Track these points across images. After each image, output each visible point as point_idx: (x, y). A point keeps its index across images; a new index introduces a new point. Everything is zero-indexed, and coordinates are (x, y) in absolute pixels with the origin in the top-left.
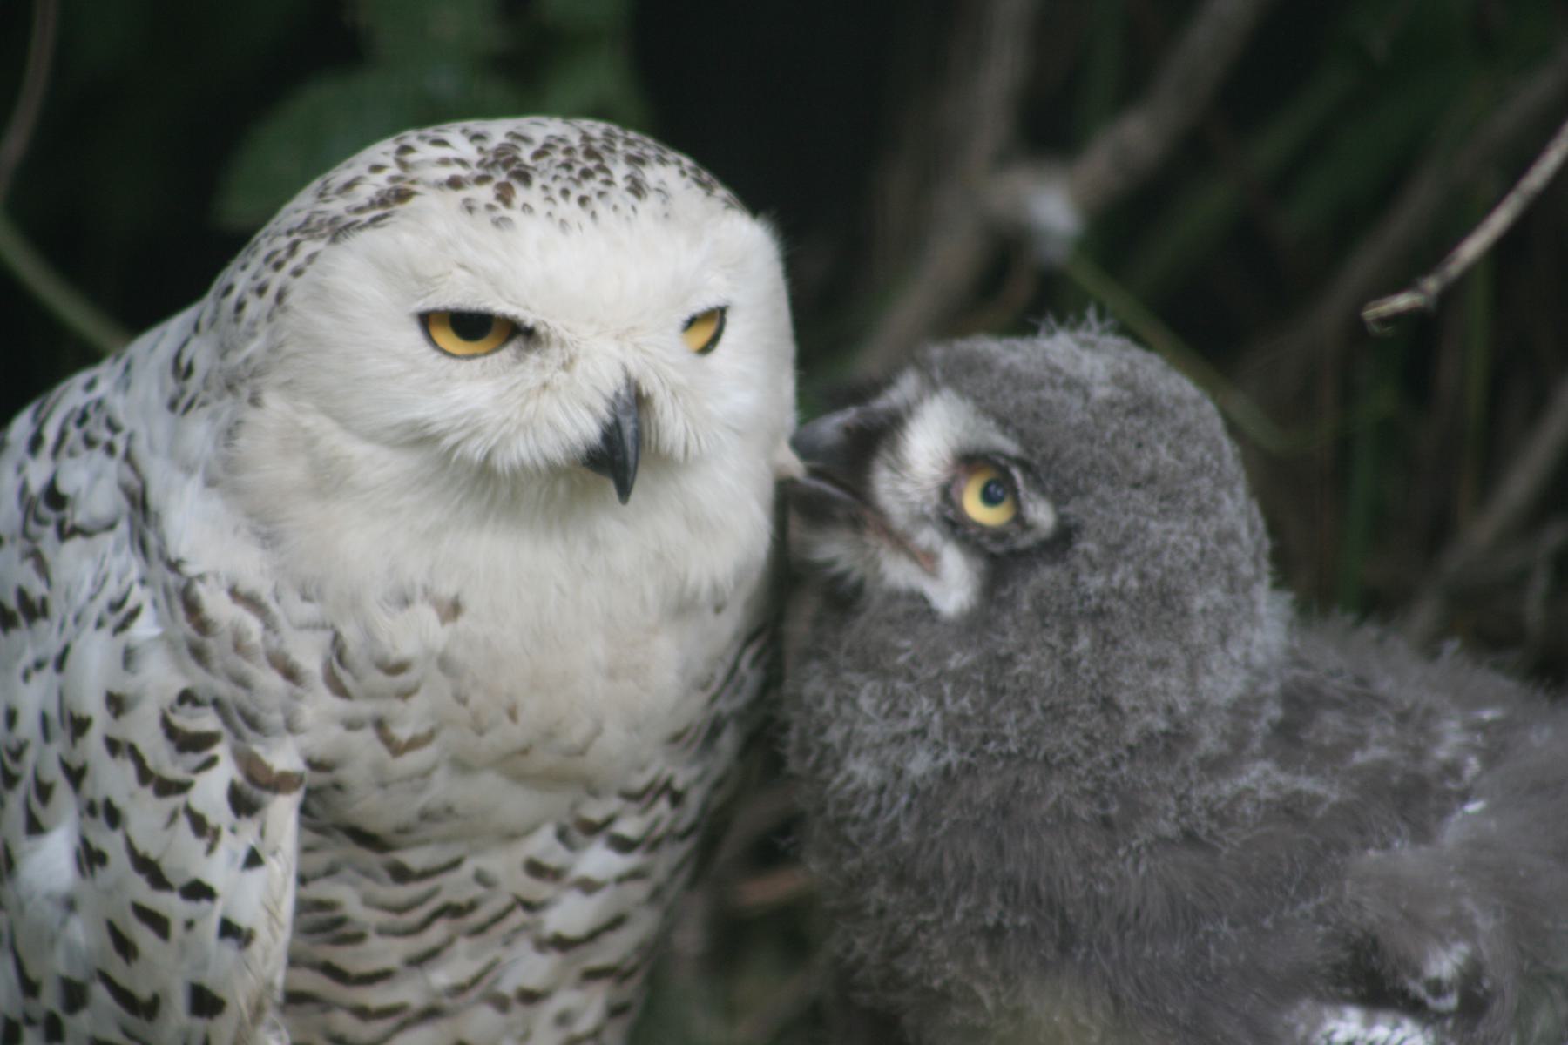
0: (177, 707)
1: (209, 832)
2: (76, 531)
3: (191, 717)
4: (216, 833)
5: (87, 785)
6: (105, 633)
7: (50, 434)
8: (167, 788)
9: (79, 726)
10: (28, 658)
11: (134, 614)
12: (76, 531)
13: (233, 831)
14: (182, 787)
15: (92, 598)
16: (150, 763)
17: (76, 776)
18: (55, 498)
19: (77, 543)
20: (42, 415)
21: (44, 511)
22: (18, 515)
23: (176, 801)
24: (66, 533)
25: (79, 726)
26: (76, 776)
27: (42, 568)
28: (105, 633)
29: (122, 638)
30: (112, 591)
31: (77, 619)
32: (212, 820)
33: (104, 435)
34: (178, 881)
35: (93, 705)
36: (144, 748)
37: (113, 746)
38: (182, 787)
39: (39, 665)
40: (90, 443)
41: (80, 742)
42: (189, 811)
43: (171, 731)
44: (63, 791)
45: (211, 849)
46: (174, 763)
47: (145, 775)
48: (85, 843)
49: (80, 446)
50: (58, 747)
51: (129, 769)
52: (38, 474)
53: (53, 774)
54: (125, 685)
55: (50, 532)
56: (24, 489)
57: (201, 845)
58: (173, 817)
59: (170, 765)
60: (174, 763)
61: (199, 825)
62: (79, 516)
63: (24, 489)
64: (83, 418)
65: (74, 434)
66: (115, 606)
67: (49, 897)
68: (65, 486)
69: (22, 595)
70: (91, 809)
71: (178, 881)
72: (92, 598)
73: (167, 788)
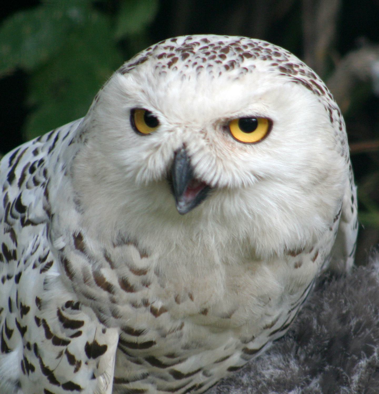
0: (65, 308)
1: (76, 363)
2: (30, 222)
3: (71, 314)
4: (79, 364)
5: (26, 334)
6: (37, 270)
7: (18, 173)
8: (58, 342)
9: (25, 310)
10: (5, 273)
11: (50, 264)
12: (30, 222)
13: (86, 363)
14: (66, 343)
15: (32, 254)
16: (51, 330)
17: (23, 330)
18: (20, 207)
19: (29, 228)
20: (14, 162)
21: (15, 211)
22: (3, 211)
23: (63, 348)
24: (25, 223)
25: (25, 310)
26: (23, 330)
27: (14, 237)
28: (37, 270)
29: (44, 274)
30: (40, 252)
31: (25, 262)
32: (77, 358)
33: (42, 179)
34: (62, 382)
35: (30, 302)
36: (49, 323)
37: (37, 320)
38: (66, 343)
39: (9, 277)
40: (36, 183)
41: (24, 316)
42: (67, 352)
43: (61, 318)
44: (16, 333)
45: (76, 370)
46: (62, 332)
47: (49, 334)
48: (25, 359)
49: (32, 184)
50: (16, 314)
51: (42, 331)
52: (13, 196)
53: (12, 326)
54: (44, 296)
55: (18, 222)
56: (6, 199)
57: (73, 368)
58: (60, 355)
59: (62, 334)
60: (62, 332)
61: (71, 359)
62: (31, 216)
63: (6, 199)
64: (32, 170)
65: (29, 177)
66: (42, 260)
67: (9, 380)
68: (25, 202)
69: (4, 247)
70: (28, 346)
71: (62, 382)
72: (32, 254)
73: (58, 342)
